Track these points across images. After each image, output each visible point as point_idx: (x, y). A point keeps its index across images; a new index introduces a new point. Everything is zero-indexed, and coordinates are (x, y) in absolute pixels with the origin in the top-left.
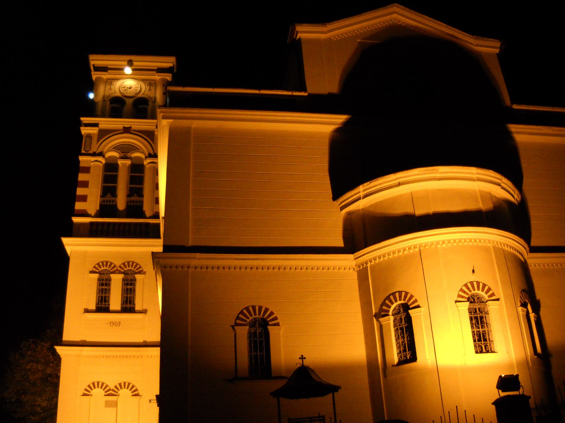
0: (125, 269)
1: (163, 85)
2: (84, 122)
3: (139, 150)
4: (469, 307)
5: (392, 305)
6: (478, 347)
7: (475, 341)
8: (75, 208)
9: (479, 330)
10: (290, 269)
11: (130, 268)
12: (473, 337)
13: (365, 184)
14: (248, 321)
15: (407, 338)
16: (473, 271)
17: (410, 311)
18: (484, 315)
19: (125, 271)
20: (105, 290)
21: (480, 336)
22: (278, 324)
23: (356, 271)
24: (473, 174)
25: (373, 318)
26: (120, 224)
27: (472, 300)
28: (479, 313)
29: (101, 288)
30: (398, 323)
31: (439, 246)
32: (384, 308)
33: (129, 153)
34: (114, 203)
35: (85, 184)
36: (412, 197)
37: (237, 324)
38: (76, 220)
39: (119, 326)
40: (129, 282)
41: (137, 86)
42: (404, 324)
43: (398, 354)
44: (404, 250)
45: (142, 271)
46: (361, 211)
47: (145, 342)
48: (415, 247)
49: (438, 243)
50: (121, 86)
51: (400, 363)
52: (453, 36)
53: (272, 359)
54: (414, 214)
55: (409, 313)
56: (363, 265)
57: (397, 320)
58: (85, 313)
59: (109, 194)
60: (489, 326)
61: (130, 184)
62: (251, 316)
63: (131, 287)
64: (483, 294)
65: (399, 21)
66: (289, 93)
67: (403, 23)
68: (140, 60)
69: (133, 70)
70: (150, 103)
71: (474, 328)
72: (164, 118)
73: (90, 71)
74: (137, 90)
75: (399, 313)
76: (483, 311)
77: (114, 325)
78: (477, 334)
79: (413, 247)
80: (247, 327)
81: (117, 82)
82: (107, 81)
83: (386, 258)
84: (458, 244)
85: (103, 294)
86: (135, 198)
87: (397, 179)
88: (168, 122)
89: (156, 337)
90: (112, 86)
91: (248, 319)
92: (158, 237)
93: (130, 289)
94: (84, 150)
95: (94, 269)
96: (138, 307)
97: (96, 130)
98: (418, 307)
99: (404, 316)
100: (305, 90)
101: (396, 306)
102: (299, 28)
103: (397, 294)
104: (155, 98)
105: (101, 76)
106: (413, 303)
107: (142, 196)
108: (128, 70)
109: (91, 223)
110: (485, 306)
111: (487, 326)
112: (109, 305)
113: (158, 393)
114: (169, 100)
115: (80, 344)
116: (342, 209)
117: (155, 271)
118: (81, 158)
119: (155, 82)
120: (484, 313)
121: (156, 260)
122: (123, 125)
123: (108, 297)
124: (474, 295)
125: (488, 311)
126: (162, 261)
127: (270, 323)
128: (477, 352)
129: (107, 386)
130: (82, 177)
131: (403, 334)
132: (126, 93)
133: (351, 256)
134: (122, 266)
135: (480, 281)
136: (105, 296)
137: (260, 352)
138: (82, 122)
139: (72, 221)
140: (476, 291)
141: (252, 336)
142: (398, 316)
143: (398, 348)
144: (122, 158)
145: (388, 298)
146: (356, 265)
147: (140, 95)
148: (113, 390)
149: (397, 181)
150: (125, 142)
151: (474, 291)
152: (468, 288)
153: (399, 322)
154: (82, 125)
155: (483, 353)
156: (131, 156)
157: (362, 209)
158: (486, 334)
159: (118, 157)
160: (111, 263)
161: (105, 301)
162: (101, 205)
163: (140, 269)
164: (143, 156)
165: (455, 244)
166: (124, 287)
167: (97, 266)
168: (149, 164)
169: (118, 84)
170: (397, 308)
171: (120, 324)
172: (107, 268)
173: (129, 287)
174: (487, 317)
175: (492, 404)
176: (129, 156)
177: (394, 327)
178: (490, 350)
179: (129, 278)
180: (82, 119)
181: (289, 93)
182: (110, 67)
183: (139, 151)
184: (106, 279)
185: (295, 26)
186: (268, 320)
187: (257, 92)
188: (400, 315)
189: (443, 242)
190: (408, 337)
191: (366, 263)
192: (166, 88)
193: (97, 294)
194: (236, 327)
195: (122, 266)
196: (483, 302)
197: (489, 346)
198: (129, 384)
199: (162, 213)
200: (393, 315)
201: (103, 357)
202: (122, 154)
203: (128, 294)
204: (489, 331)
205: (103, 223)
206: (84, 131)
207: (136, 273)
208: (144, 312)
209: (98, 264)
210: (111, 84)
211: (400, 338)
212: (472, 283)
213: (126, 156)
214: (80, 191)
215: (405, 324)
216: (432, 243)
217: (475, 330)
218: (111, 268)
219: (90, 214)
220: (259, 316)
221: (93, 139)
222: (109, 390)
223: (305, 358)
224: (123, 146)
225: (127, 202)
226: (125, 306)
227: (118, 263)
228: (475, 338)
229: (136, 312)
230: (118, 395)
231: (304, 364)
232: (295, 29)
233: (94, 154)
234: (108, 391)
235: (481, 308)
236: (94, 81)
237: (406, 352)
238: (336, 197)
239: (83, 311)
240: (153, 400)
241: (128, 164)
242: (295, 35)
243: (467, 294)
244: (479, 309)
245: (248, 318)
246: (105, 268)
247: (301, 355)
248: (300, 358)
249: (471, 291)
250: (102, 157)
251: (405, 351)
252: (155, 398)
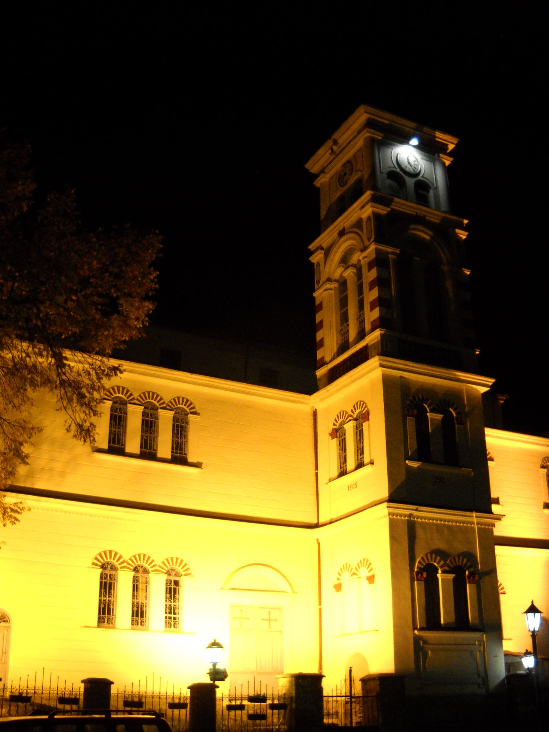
9: (171, 603)
21: (171, 610)
27: (103, 567)
40: (180, 424)
148: (160, 566)
175: (82, 682)
201: (376, 520)
227: (167, 398)
243: (103, 559)
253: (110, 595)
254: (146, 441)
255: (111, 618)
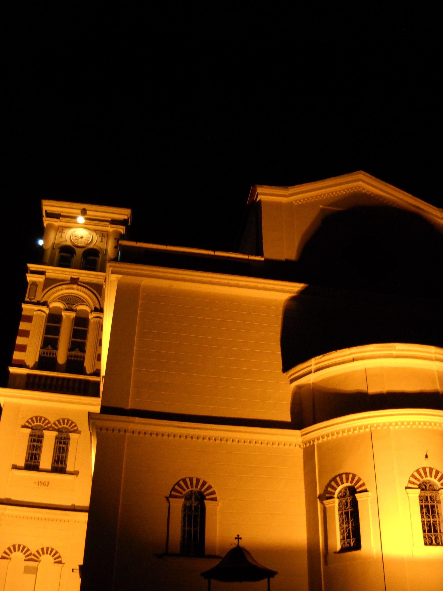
0: (60, 427)
1: (115, 239)
2: (30, 269)
3: (85, 302)
4: (420, 495)
5: (338, 487)
6: (427, 538)
7: (424, 531)
8: (12, 358)
9: (429, 520)
10: (233, 441)
11: (65, 426)
12: (423, 527)
13: (318, 357)
14: (184, 493)
15: (352, 523)
16: (427, 456)
17: (357, 495)
18: (435, 505)
19: (59, 429)
20: (36, 447)
22: (215, 499)
23: (302, 448)
24: (431, 353)
25: (317, 502)
26: (58, 378)
27: (423, 487)
28: (431, 536)
29: (32, 444)
30: (343, 507)
31: (391, 427)
32: (329, 489)
33: (74, 304)
34: (54, 356)
35: (26, 334)
36: (366, 373)
37: (171, 496)
38: (12, 370)
39: (47, 486)
41: (89, 236)
42: (349, 508)
43: (341, 540)
44: (355, 429)
45: (77, 430)
46: (312, 385)
47: (74, 506)
48: (366, 427)
49: (390, 424)
50: (73, 234)
51: (344, 550)
52: (418, 208)
53: (206, 536)
54: (367, 392)
55: (355, 497)
56: (310, 442)
57: (342, 503)
58: (12, 469)
59: (50, 346)
60: (440, 516)
61: (73, 338)
62: (188, 488)
63: (64, 446)
64: (436, 481)
65: (364, 189)
66: (245, 257)
67: (368, 191)
68: (94, 209)
69: (87, 219)
70: (101, 256)
71: (424, 517)
72: (113, 272)
73: (42, 216)
74: (88, 241)
75: (345, 496)
76: (435, 500)
77: (43, 484)
78: (427, 524)
79: (363, 427)
80: (183, 500)
81: (69, 230)
82: (58, 229)
83: (335, 437)
84: (411, 426)
85: (34, 451)
86: (77, 353)
87: (351, 354)
88: (117, 278)
89: (85, 502)
90: (63, 233)
91: (184, 491)
92: (97, 396)
93: (63, 448)
94: (28, 297)
95: (27, 424)
96: (69, 468)
97: (43, 278)
98: (366, 491)
99: (350, 499)
100: (262, 255)
101: (343, 489)
102: (260, 190)
103: (344, 477)
104: (106, 250)
105: (52, 222)
106: (361, 486)
107: (83, 351)
108: (81, 220)
109: (29, 375)
110: (437, 494)
111: (438, 516)
112: (39, 463)
113: (81, 563)
114: (120, 253)
115: (4, 502)
116: (292, 381)
117: (91, 433)
118: (24, 306)
119: (108, 233)
120: (435, 502)
121: (92, 421)
122: (71, 275)
123: (39, 454)
124: (426, 481)
125: (440, 500)
126: (99, 423)
127: (207, 497)
128: (426, 544)
129: (28, 550)
130: (23, 326)
131: (348, 519)
132: (77, 243)
133: (297, 433)
134: (57, 423)
135: (432, 468)
136: (35, 454)
137: (194, 527)
138: (28, 269)
139: (8, 372)
140: (429, 478)
141: (187, 509)
142: (344, 499)
143: (342, 533)
144: (66, 310)
145: (334, 479)
146: (302, 442)
147: (91, 246)
149: (352, 356)
150: (71, 293)
151: (426, 477)
152: (420, 474)
153: (344, 506)
154: (29, 272)
155: (433, 545)
156: (76, 309)
157: (312, 383)
158: (436, 525)
159: (62, 309)
160: (45, 419)
161: (35, 458)
162: (40, 357)
163: (75, 428)
164: (89, 310)
165: (409, 426)
166: (56, 445)
167: (30, 421)
168: (93, 319)
169: (69, 233)
170: (343, 491)
171: (48, 484)
172: (41, 424)
173: (62, 446)
174: (438, 507)
176: (75, 308)
177: (339, 511)
178: (440, 542)
179: (63, 436)
180: (29, 265)
181: (245, 257)
182: (62, 214)
183: (85, 304)
184: (38, 435)
185: (256, 187)
186: (205, 493)
187: (211, 253)
188: (346, 498)
189: (396, 424)
190: (352, 502)
191: (314, 441)
192: (118, 242)
193: (27, 450)
194: (171, 499)
195: (57, 423)
196: (435, 490)
197: (439, 538)
198: (52, 550)
199: (103, 372)
200: (338, 498)
202: (67, 306)
203: (60, 453)
204: (440, 521)
205: (41, 377)
206: (30, 278)
207: (71, 432)
208: (76, 473)
209: (32, 419)
210: (62, 232)
211: (344, 523)
212: (424, 469)
213: (71, 308)
214: (20, 340)
215: (350, 509)
216: (384, 424)
217: (426, 520)
218: (45, 423)
219: (28, 365)
220: (196, 489)
221: (38, 287)
222: (31, 554)
223: (241, 538)
224: (69, 297)
225: (68, 356)
226: (56, 465)
227: (52, 419)
228: (425, 528)
229: (67, 472)
230: (40, 561)
231: (240, 545)
232: (256, 190)
233: (38, 303)
234: (28, 556)
235: (433, 497)
236: (45, 227)
237: (350, 538)
238: (285, 369)
239: (11, 467)
240: (76, 569)
241: (72, 316)
242: (255, 198)
243: (419, 480)
244: (430, 497)
245: (184, 490)
246: (38, 423)
247: (237, 535)
248: (236, 538)
249: (423, 478)
250: (46, 307)
251: (348, 537)
252: (78, 568)
253: (434, 514)
254: (59, 457)
255: (439, 536)
